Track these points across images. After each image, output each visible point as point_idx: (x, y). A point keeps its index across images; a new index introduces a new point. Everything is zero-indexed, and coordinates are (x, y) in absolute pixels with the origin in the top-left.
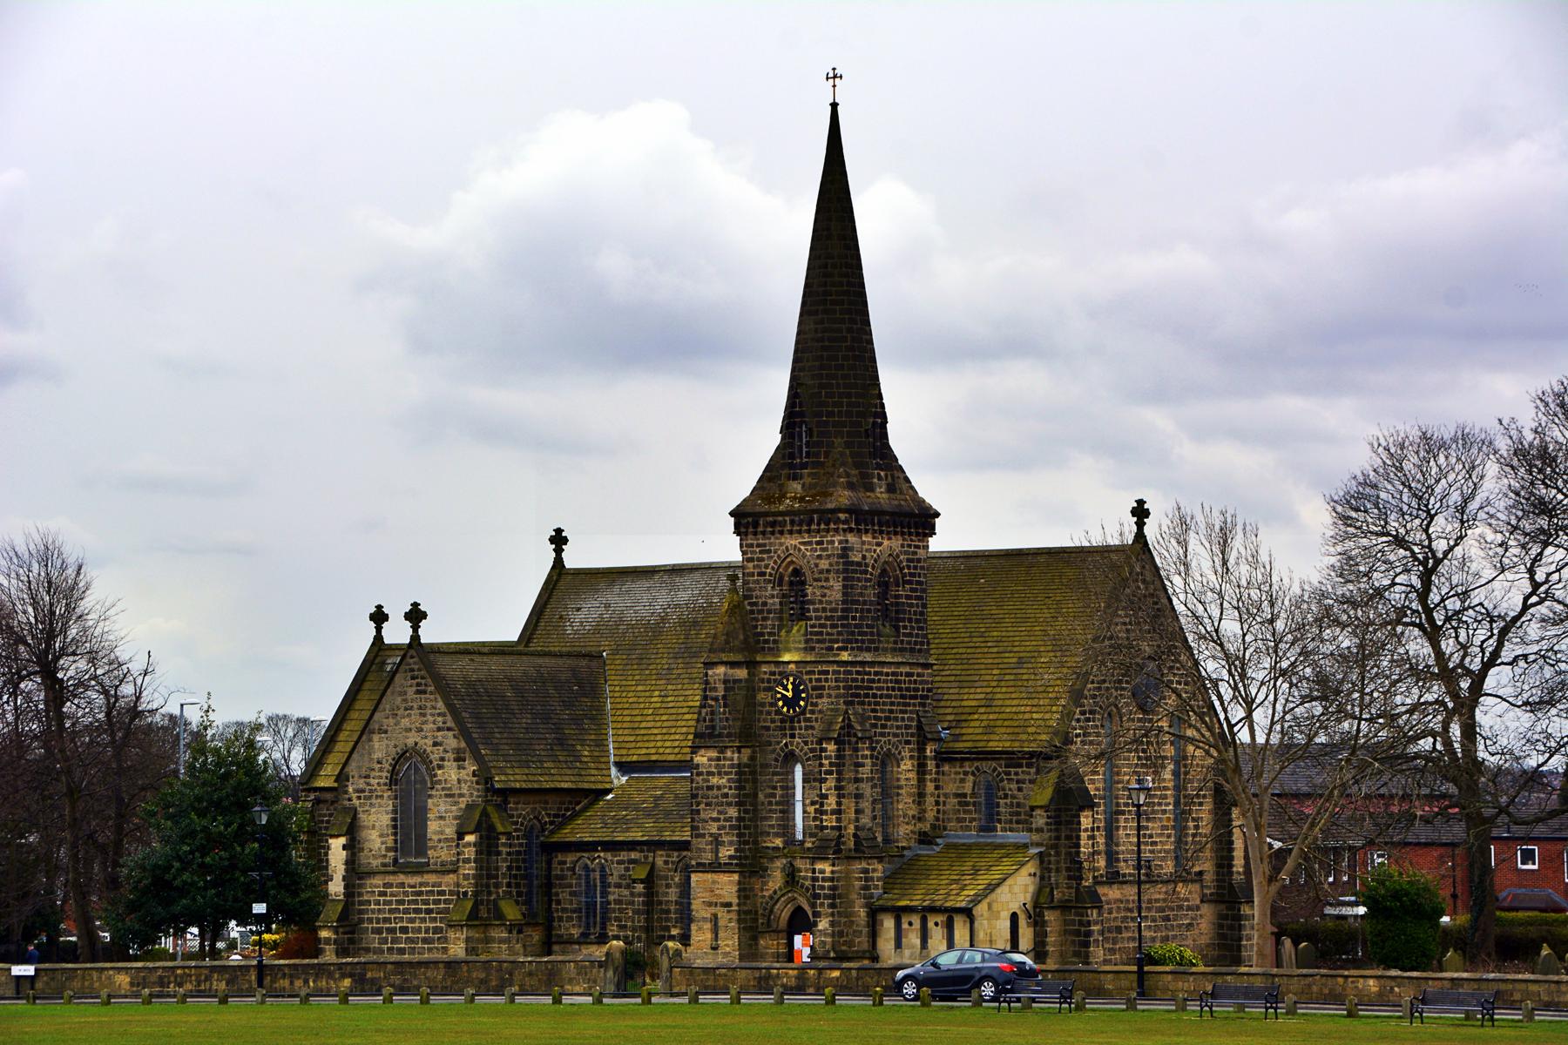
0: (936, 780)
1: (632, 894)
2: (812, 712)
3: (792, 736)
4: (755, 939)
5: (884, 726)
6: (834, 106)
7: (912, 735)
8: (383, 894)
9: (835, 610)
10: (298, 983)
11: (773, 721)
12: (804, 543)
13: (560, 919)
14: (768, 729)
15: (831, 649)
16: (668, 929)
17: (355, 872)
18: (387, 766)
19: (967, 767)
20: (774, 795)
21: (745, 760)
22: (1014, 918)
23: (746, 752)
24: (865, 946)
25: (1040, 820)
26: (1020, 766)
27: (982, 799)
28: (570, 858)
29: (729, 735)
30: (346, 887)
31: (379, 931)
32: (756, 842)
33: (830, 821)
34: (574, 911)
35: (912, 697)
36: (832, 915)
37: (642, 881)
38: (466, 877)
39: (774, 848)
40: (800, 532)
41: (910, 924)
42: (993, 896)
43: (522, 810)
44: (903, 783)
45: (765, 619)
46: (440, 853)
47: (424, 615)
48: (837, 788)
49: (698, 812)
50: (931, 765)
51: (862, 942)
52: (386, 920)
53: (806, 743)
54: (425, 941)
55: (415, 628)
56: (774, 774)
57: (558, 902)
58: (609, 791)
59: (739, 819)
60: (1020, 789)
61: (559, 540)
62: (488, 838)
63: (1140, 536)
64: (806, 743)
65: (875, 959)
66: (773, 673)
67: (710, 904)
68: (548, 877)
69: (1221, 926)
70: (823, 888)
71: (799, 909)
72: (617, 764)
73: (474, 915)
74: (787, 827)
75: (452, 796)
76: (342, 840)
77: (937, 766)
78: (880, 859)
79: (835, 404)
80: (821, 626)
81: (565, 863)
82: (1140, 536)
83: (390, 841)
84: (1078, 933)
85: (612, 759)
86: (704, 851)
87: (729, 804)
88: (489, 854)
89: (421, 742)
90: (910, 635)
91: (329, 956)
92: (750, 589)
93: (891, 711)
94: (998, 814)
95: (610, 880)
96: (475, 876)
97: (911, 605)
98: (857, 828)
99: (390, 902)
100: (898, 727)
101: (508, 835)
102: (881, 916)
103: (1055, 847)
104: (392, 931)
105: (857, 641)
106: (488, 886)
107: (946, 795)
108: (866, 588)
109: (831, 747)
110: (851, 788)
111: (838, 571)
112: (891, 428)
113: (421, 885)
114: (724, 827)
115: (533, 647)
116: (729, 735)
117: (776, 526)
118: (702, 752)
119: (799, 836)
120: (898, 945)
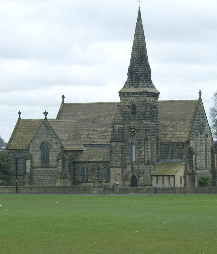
2: (138, 134)
3: (133, 139)
4: (124, 181)
7: (156, 139)
8: (39, 172)
12: (135, 99)
14: (127, 138)
16: (102, 179)
17: (32, 168)
18: (39, 145)
27: (170, 153)
28: (79, 165)
29: (119, 139)
31: (38, 180)
33: (142, 157)
34: (80, 176)
36: (143, 177)
37: (97, 170)
38: (59, 169)
42: (178, 173)
43: (69, 154)
46: (52, 163)
48: (144, 150)
50: (159, 145)
53: (136, 141)
54: (49, 182)
55: (46, 116)
59: (122, 157)
63: (200, 98)
65: (152, 186)
67: (115, 174)
74: (131, 159)
76: (30, 161)
79: (141, 70)
81: (77, 166)
82: (200, 98)
83: (40, 161)
84: (192, 180)
87: (120, 154)
89: (47, 140)
90: (155, 118)
96: (61, 169)
97: (155, 112)
98: (148, 159)
100: (154, 137)
102: (153, 177)
109: (143, 142)
113: (48, 170)
114: (118, 158)
118: (113, 142)
119: (134, 160)
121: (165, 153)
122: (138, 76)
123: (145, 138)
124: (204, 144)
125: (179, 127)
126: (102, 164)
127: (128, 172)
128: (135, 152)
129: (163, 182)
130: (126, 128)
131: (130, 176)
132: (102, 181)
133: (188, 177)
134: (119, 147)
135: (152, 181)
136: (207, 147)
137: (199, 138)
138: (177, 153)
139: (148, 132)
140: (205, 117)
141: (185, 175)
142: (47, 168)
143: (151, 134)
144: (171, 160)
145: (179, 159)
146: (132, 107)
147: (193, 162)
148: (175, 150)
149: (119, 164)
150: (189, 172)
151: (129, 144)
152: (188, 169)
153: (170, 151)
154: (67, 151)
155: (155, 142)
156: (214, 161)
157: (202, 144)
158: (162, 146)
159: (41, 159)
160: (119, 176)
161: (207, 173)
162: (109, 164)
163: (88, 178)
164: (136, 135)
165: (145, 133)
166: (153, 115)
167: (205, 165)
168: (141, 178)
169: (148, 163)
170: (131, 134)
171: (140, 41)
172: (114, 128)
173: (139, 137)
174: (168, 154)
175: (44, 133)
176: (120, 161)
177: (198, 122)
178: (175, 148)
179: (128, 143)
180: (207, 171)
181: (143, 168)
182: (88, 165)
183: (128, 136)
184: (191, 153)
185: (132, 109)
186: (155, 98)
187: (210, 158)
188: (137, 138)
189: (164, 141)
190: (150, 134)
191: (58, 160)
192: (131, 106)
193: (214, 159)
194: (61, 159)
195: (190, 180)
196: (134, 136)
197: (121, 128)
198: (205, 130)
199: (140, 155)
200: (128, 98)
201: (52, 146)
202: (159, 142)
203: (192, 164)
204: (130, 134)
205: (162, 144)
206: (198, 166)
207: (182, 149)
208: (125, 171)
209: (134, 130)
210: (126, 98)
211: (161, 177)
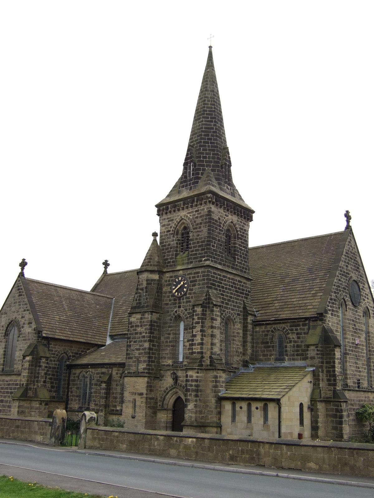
2: (190, 294)
3: (179, 307)
4: (155, 413)
5: (227, 304)
6: (210, 47)
7: (241, 312)
9: (204, 241)
11: (170, 300)
12: (189, 213)
13: (72, 400)
14: (167, 304)
20: (168, 338)
22: (301, 405)
25: (312, 352)
26: (299, 325)
27: (277, 344)
28: (78, 371)
32: (158, 362)
33: (197, 349)
34: (77, 396)
35: (241, 293)
36: (196, 401)
38: (24, 376)
39: (167, 365)
40: (187, 208)
41: (241, 408)
42: (291, 393)
43: (58, 348)
46: (17, 367)
48: (201, 331)
50: (250, 327)
53: (186, 310)
56: (170, 327)
57: (72, 392)
58: (104, 346)
59: (150, 349)
61: (106, 264)
63: (348, 227)
70: (191, 385)
72: (110, 336)
74: (175, 356)
77: (253, 328)
78: (224, 371)
80: (196, 250)
82: (348, 227)
84: (335, 416)
85: (108, 334)
87: (145, 341)
90: (240, 263)
93: (231, 297)
94: (286, 351)
97: (241, 249)
98: (212, 353)
100: (234, 306)
101: (47, 358)
105: (214, 258)
106: (34, 381)
109: (199, 310)
110: (210, 331)
111: (206, 223)
112: (232, 168)
113: (10, 380)
114: (142, 353)
116: (147, 306)
118: (134, 315)
121: (265, 347)
122: (199, 165)
124: (362, 330)
125: (299, 287)
126: (116, 369)
127: (165, 388)
130: (166, 281)
131: (170, 401)
132: (115, 409)
133: (321, 406)
134: (145, 325)
135: (220, 413)
136: (369, 340)
137: (349, 314)
138: (294, 346)
139: (216, 289)
140: (361, 272)
141: (313, 401)
142: (10, 375)
144: (278, 364)
145: (297, 360)
148: (289, 338)
149: (143, 367)
150: (326, 394)
152: (321, 385)
153: (276, 340)
154: (49, 340)
157: (356, 329)
158: (258, 330)
164: (188, 296)
166: (236, 254)
167: (367, 382)
169: (212, 366)
170: (176, 294)
171: (209, 101)
173: (192, 300)
174: (271, 348)
176: (147, 359)
177: (346, 276)
178: (288, 334)
179: (169, 318)
181: (197, 377)
182: (92, 373)
183: (170, 300)
184: (328, 342)
185: (182, 238)
186: (238, 218)
188: (188, 304)
190: (222, 294)
194: (28, 356)
195: (327, 415)
196: (183, 299)
197: (155, 280)
198: (364, 300)
200: (175, 214)
201: (22, 329)
202: (250, 319)
203: (334, 371)
205: (256, 323)
206: (350, 382)
207: (305, 333)
209: (182, 283)
210: (172, 216)
211: (244, 405)
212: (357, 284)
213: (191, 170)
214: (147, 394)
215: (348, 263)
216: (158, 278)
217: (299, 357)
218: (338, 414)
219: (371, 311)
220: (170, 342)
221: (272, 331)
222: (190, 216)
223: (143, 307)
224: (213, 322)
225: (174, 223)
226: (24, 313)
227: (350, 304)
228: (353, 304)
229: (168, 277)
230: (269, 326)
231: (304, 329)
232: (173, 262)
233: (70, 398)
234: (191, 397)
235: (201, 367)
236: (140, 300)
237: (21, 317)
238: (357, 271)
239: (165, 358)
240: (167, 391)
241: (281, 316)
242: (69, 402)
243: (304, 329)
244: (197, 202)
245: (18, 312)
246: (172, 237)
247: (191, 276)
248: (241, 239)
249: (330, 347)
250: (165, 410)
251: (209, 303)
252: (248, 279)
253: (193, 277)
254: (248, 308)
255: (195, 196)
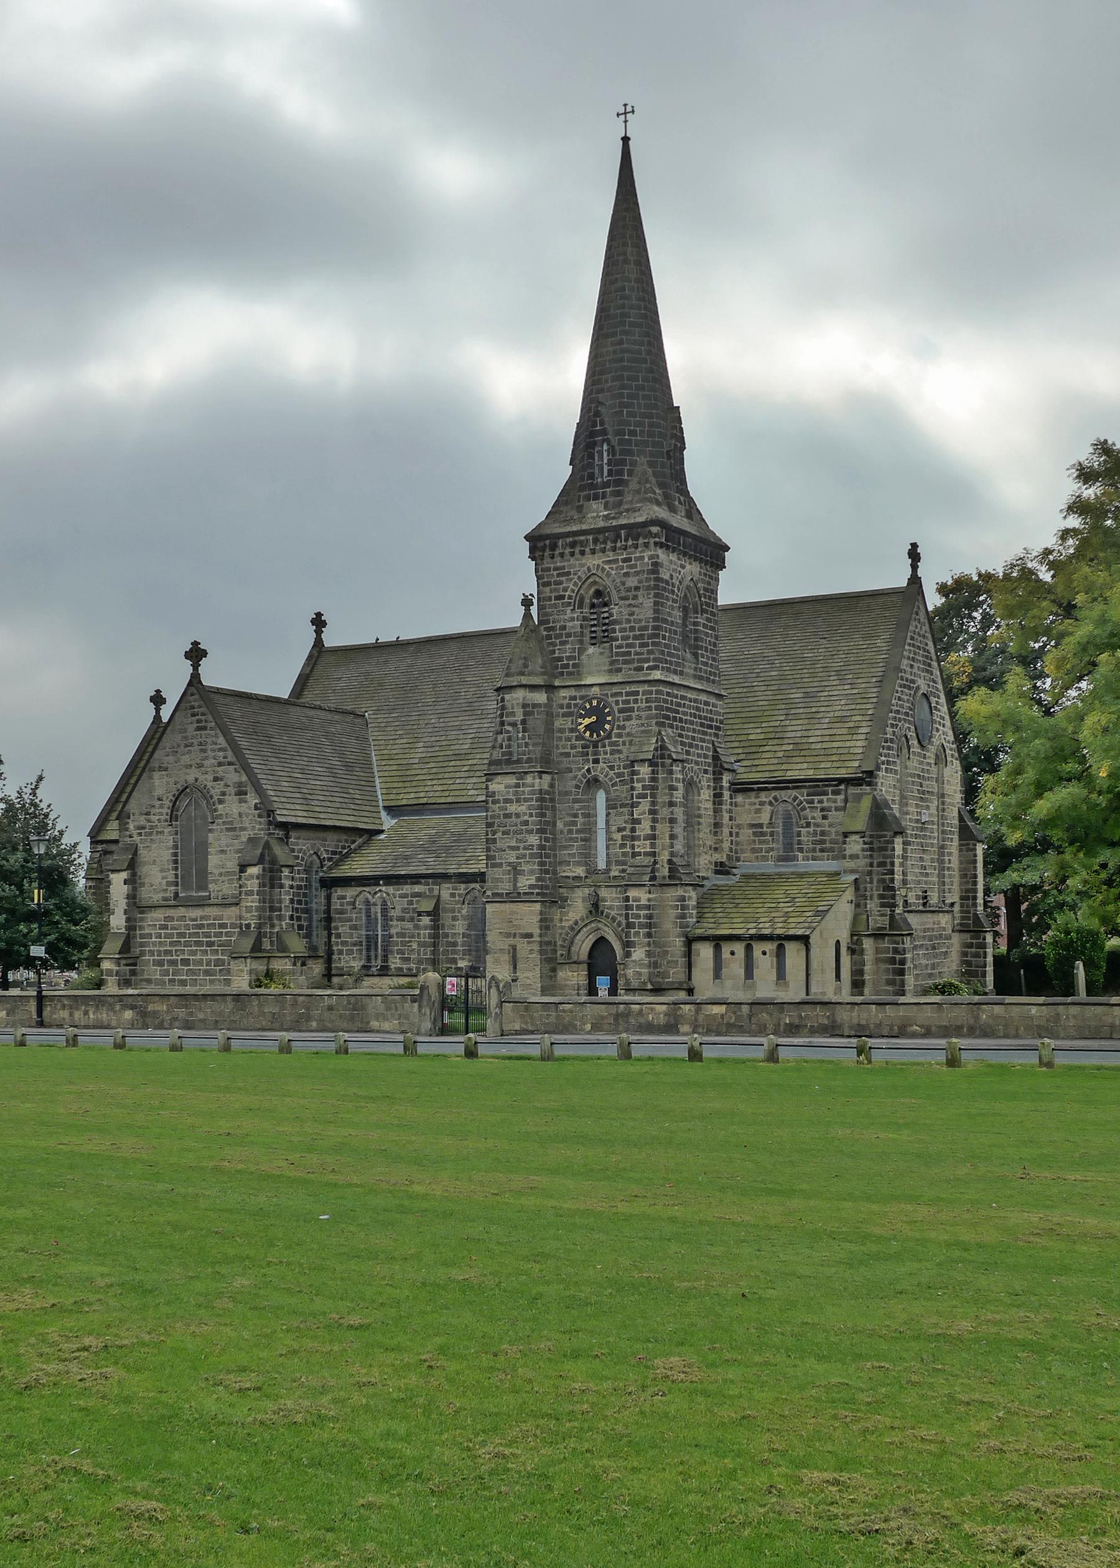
0: (730, 811)
1: (417, 927)
2: (619, 735)
3: (596, 761)
4: (554, 970)
6: (626, 140)
8: (165, 927)
9: (645, 628)
10: (78, 1015)
11: (573, 747)
12: (609, 562)
13: (341, 952)
14: (568, 755)
15: (641, 669)
18: (167, 803)
19: (764, 797)
20: (574, 823)
21: (546, 787)
23: (547, 778)
24: (682, 977)
25: (855, 845)
26: (825, 793)
27: (780, 830)
28: (350, 892)
29: (529, 760)
30: (128, 920)
32: (555, 873)
36: (649, 944)
37: (428, 914)
38: (249, 909)
39: (575, 878)
40: (603, 551)
41: (733, 953)
43: (302, 844)
44: (702, 812)
45: (563, 643)
46: (221, 888)
47: (204, 653)
49: (494, 841)
50: (726, 794)
51: (676, 973)
52: (167, 952)
56: (575, 801)
57: (338, 936)
58: (383, 831)
59: (542, 847)
60: (824, 817)
61: (319, 622)
62: (271, 870)
63: (915, 580)
64: (612, 768)
65: (690, 991)
66: (574, 698)
67: (508, 935)
68: (328, 911)
69: (965, 954)
70: (638, 917)
71: (601, 941)
72: (385, 807)
73: (257, 947)
74: (587, 857)
75: (234, 829)
76: (124, 875)
80: (629, 646)
84: (892, 961)
86: (501, 880)
87: (530, 832)
88: (272, 887)
89: (201, 778)
90: (706, 664)
91: (111, 988)
92: (546, 614)
93: (693, 738)
94: (799, 842)
95: (392, 913)
96: (258, 909)
97: (707, 634)
98: (672, 854)
99: (170, 936)
100: (699, 756)
102: (696, 946)
103: (870, 873)
104: (173, 963)
106: (270, 918)
107: (739, 826)
108: (673, 608)
109: (645, 770)
111: (648, 588)
113: (202, 918)
114: (524, 856)
115: (308, 697)
116: (529, 760)
117: (576, 543)
118: (499, 779)
119: (602, 865)
120: (717, 974)
123: (656, 749)
127: (571, 923)
128: (607, 822)
129: (749, 973)
131: (583, 946)
133: (868, 944)
136: (943, 810)
137: (914, 764)
138: (815, 833)
139: (671, 726)
143: (687, 737)
146: (593, 606)
147: (893, 874)
149: (528, 883)
150: (876, 922)
151: (577, 787)
155: (705, 781)
156: (975, 876)
157: (923, 793)
159: (176, 869)
160: (529, 943)
161: (944, 929)
162: (482, 887)
163: (392, 952)
165: (655, 729)
168: (638, 954)
170: (588, 734)
172: (503, 708)
173: (624, 749)
175: (186, 746)
177: (910, 688)
178: (804, 809)
179: (574, 783)
180: (944, 920)
181: (649, 900)
182: (388, 894)
184: (882, 826)
187: (955, 863)
188: (616, 756)
189: (751, 775)
190: (681, 736)
191: (243, 868)
192: (587, 601)
193: (975, 868)
194: (255, 865)
195: (878, 961)
196: (604, 746)
197: (539, 705)
199: (633, 838)
201: (220, 807)
202: (726, 778)
203: (892, 880)
204: (583, 738)
207: (837, 809)
208: (561, 920)
211: (739, 948)
212: (928, 699)
213: (605, 461)
214: (541, 935)
215: (913, 659)
216: (546, 701)
217: (825, 854)
218: (898, 957)
219: (947, 751)
220: (578, 831)
221: (771, 803)
222: (612, 568)
223: (519, 761)
224: (672, 795)
225: (571, 579)
226: (219, 769)
227: (916, 742)
228: (919, 742)
229: (565, 698)
230: (763, 794)
231: (835, 801)
232: (574, 665)
233: (335, 948)
234: (639, 936)
235: (656, 883)
236: (509, 746)
237: (211, 778)
238: (927, 671)
239: (568, 863)
240: (577, 928)
241: (789, 773)
242: (335, 957)
243: (835, 801)
244: (626, 540)
245: (202, 766)
246: (569, 611)
247: (620, 699)
248: (706, 612)
249: (885, 836)
250: (575, 963)
251: (662, 757)
252: (719, 696)
253: (624, 702)
254: (723, 758)
255: (622, 527)
